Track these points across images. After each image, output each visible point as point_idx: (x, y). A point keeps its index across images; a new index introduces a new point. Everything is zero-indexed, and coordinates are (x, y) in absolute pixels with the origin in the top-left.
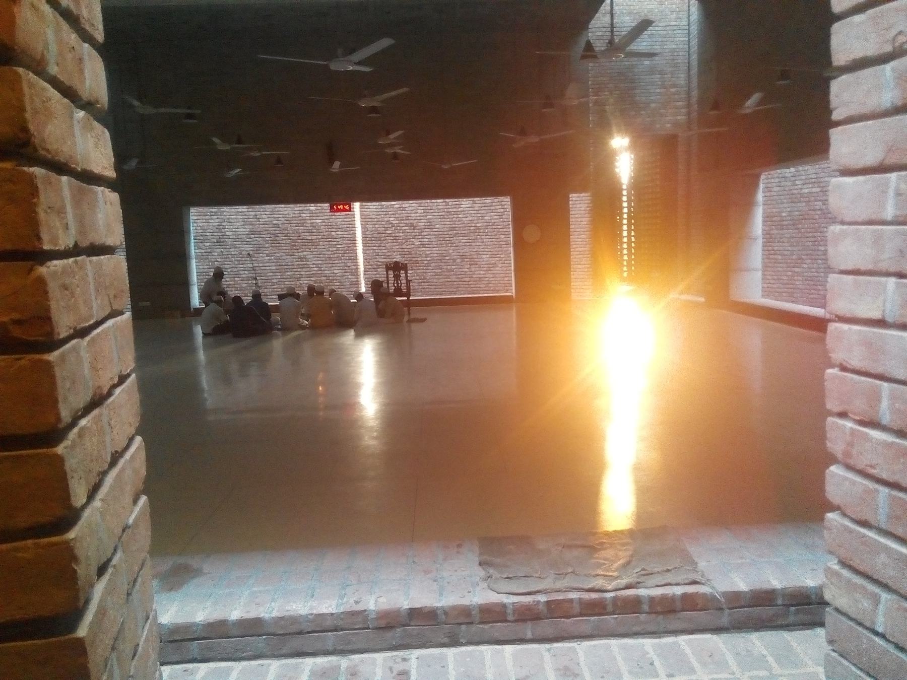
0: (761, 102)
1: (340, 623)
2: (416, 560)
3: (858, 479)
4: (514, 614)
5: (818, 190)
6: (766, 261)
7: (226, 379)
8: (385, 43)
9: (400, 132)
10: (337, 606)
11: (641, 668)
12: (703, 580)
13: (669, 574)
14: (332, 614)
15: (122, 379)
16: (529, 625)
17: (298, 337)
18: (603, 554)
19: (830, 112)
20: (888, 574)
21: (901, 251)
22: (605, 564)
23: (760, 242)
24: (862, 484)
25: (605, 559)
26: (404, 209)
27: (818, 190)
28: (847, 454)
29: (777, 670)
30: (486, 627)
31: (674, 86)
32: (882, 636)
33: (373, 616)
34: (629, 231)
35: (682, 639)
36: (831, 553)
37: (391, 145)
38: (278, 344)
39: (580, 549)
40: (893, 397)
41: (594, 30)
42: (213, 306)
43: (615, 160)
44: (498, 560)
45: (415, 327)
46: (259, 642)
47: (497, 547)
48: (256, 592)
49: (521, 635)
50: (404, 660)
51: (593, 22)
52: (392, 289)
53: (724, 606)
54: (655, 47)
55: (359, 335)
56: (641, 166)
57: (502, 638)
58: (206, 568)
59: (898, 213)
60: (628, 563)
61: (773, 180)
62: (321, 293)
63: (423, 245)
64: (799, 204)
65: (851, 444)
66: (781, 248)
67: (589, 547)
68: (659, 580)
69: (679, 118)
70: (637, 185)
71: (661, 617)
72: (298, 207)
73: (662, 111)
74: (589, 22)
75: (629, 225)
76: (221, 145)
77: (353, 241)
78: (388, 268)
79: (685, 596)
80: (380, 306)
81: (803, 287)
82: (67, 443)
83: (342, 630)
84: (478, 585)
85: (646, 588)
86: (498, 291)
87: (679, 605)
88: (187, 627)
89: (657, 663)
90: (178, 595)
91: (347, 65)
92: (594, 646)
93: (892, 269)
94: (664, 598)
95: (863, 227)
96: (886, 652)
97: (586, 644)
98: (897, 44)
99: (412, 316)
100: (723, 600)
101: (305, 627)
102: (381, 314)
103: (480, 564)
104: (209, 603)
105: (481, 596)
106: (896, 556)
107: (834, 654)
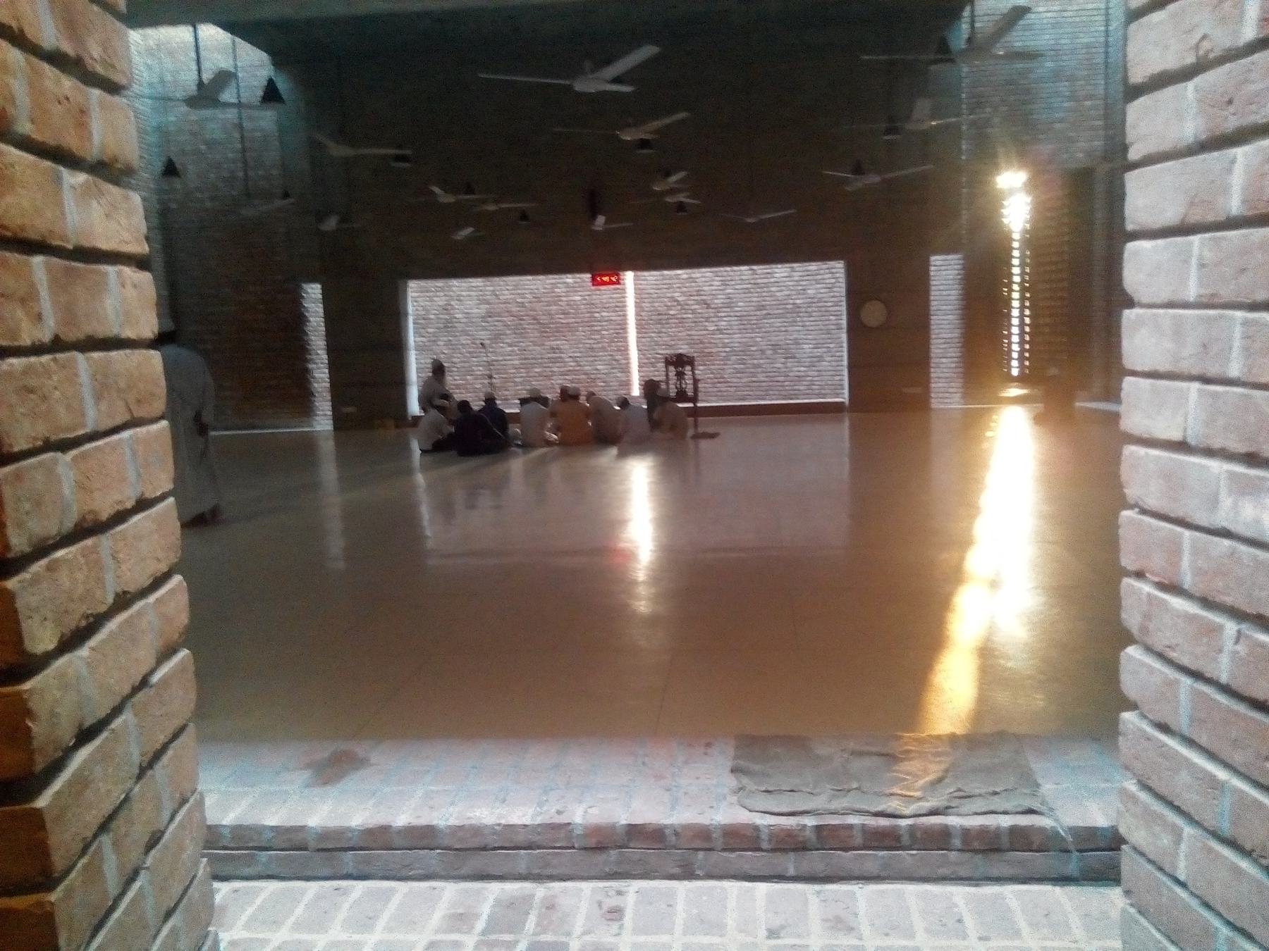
1: (536, 838)
2: (646, 759)
3: (1157, 665)
4: (770, 841)
7: (446, 510)
8: (647, 51)
10: (533, 816)
12: (1043, 809)
13: (996, 798)
15: (143, 504)
16: (792, 855)
17: (545, 455)
18: (906, 766)
19: (1125, 148)
20: (1190, 798)
21: (1204, 346)
22: (905, 780)
24: (1162, 673)
26: (693, 280)
28: (1144, 630)
30: (733, 855)
32: (1183, 885)
33: (578, 832)
34: (1022, 308)
35: (1010, 891)
36: (1127, 768)
37: (672, 191)
38: (517, 465)
39: (874, 758)
40: (1196, 552)
42: (434, 413)
43: (1002, 206)
45: (704, 444)
46: (432, 858)
48: (432, 791)
49: (779, 870)
50: (620, 893)
53: (1072, 847)
54: (1063, 41)
55: (623, 455)
56: (1041, 212)
57: (754, 873)
58: (375, 757)
59: (1203, 291)
62: (576, 397)
63: (720, 331)
65: (1147, 616)
68: (979, 805)
70: (1033, 240)
72: (550, 279)
75: (1022, 299)
76: (445, 198)
77: (623, 326)
79: (1014, 830)
80: (655, 415)
82: (25, 576)
84: (725, 798)
85: (958, 815)
86: (824, 396)
87: (1005, 842)
88: (340, 833)
90: (333, 791)
91: (588, 85)
92: (883, 891)
93: (1195, 371)
94: (983, 832)
95: (1161, 311)
96: (1187, 907)
98: (1201, 53)
99: (700, 430)
101: (492, 841)
102: (655, 424)
103: (732, 771)
104: (371, 803)
105: (727, 812)
106: (1201, 776)
107: (1132, 910)
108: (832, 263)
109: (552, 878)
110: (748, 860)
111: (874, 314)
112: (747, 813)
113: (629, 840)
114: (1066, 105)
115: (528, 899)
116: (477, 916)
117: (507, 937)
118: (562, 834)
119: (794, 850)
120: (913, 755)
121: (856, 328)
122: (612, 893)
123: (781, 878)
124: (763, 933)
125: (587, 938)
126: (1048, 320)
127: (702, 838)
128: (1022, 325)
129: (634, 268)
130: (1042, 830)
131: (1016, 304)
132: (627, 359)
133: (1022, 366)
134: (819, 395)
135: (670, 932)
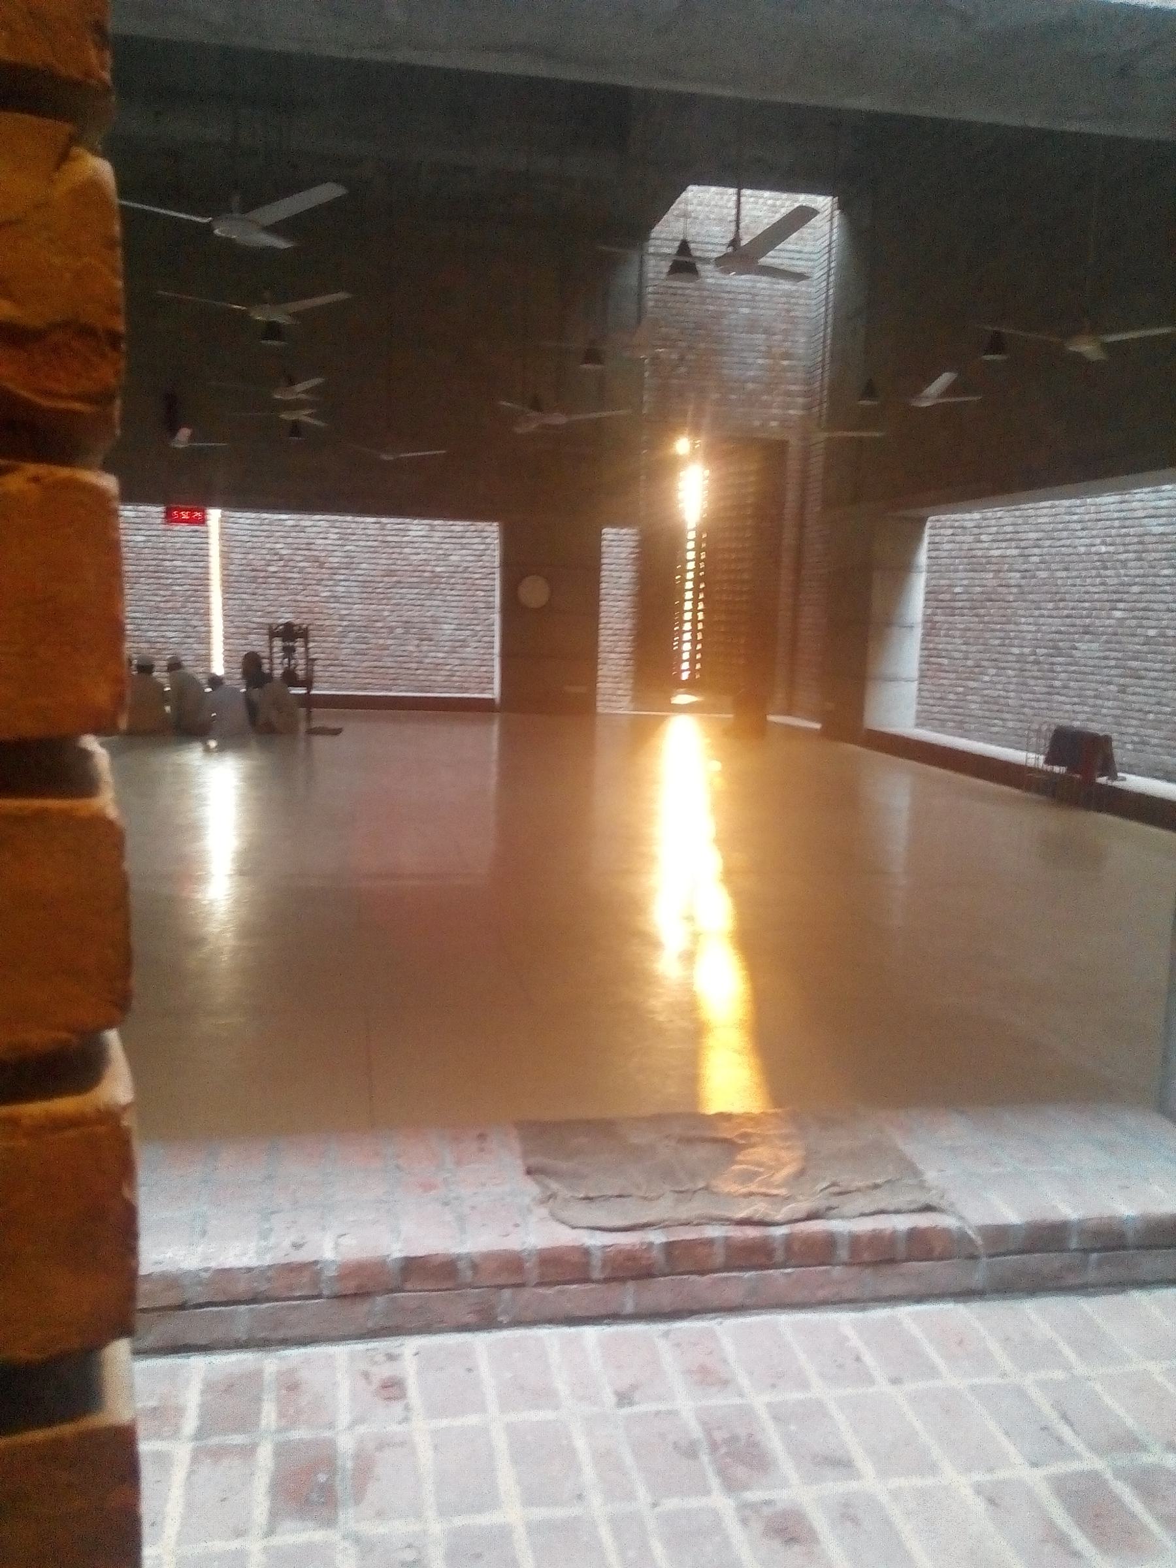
0: (950, 390)
1: (264, 1287)
4: (604, 1266)
5: (1015, 552)
6: (925, 667)
9: (317, 381)
10: (260, 1253)
11: (840, 1366)
12: (943, 1204)
14: (249, 1270)
16: (631, 1286)
22: (760, 1174)
23: (918, 632)
25: (760, 1165)
27: (1015, 552)
29: (1081, 1369)
30: (550, 1291)
31: (787, 356)
33: (331, 1272)
34: (695, 601)
35: (905, 1313)
41: (658, 242)
44: (563, 1165)
45: (320, 742)
47: (564, 1137)
49: (613, 1308)
50: (391, 1357)
51: (657, 228)
52: (278, 672)
53: (982, 1251)
60: (802, 1173)
61: (942, 531)
64: (983, 575)
66: (949, 647)
67: (725, 1141)
68: (862, 1203)
69: (791, 412)
71: (868, 1271)
73: (765, 397)
74: (651, 227)
75: (696, 591)
78: (273, 634)
79: (914, 1235)
81: (980, 713)
83: (268, 1299)
84: (530, 1211)
85: (842, 1217)
86: (467, 690)
87: (901, 1249)
89: (869, 1359)
94: (876, 1240)
97: (733, 1323)
99: (316, 724)
100: (979, 1241)
101: (195, 1294)
103: (529, 1172)
105: (538, 1233)
108: (481, 525)
109: (286, 1343)
110: (575, 1295)
111: (535, 592)
112: (568, 1231)
113: (405, 1280)
114: (760, 361)
115: (255, 1376)
116: (180, 1411)
117: (238, 1439)
118: (305, 1278)
119: (633, 1278)
120: (753, 1140)
121: (512, 607)
122: (380, 1358)
123: (614, 1317)
124: (609, 1398)
125: (362, 1429)
126: (723, 617)
127: (509, 1270)
128: (694, 621)
129: (225, 504)
130: (946, 1231)
131: (689, 595)
132: (208, 625)
133: (692, 669)
134: (462, 689)
135: (481, 1408)
